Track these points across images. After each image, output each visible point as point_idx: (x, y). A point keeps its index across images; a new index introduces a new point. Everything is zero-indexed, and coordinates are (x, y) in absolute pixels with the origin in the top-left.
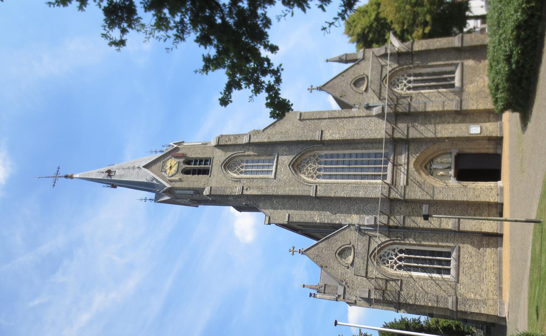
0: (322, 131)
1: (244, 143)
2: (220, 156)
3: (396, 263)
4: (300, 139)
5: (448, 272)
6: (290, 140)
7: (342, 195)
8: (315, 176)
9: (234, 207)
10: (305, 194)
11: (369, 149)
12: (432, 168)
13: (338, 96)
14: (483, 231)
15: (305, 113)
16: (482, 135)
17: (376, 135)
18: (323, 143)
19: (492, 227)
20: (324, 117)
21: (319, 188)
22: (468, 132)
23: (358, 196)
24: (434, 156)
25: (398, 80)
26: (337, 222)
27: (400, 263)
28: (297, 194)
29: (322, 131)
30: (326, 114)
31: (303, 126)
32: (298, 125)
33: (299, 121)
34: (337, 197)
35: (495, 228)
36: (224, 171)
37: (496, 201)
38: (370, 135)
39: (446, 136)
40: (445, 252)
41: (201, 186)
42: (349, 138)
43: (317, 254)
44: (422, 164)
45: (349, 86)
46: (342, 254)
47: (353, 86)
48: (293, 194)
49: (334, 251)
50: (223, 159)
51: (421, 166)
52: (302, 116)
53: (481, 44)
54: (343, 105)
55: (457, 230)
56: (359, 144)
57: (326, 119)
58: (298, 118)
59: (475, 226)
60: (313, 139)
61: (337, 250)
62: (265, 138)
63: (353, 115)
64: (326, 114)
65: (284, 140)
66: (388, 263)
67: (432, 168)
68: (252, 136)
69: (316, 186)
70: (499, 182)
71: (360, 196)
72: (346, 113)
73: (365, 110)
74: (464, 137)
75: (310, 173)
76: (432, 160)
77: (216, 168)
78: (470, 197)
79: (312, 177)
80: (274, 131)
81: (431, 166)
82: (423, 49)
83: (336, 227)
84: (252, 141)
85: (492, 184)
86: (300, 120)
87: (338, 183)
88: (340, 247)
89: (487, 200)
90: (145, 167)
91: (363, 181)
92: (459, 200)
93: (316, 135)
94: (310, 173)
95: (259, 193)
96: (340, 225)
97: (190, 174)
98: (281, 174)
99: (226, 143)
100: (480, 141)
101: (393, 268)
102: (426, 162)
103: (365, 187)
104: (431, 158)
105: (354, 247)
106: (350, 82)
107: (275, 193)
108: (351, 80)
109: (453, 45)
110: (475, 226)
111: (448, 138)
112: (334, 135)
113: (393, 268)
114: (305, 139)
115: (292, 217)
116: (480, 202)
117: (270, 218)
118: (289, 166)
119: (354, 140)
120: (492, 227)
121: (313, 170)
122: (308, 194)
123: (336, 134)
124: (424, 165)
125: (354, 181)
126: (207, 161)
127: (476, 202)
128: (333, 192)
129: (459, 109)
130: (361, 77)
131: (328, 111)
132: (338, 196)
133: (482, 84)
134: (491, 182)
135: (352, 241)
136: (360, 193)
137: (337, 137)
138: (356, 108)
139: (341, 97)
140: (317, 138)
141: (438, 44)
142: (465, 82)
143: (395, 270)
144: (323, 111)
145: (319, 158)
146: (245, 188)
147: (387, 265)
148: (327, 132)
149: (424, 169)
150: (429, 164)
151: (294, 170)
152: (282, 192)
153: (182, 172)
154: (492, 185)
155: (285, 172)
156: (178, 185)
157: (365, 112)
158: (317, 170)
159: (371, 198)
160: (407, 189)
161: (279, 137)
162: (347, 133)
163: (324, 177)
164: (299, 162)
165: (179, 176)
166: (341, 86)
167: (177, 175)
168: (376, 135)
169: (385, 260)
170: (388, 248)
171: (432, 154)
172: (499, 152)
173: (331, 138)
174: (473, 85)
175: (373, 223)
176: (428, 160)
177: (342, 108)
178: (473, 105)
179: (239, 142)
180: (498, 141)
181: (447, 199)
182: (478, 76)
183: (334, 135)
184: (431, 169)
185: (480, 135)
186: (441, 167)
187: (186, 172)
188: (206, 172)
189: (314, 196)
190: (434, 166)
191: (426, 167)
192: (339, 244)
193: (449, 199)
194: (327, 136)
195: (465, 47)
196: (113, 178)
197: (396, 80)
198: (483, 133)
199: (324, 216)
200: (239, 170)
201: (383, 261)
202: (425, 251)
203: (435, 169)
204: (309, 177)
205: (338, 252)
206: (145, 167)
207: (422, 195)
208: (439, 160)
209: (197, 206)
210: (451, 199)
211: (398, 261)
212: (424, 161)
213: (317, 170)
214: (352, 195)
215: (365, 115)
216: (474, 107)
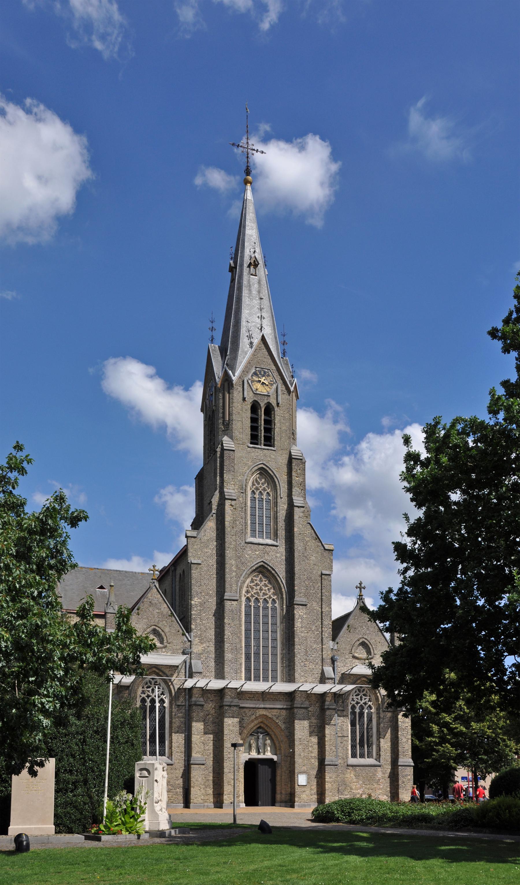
0: (306, 605)
1: (294, 498)
2: (275, 459)
3: (148, 696)
4: (296, 576)
5: (354, 756)
6: (296, 564)
7: (226, 632)
8: (249, 595)
9: (202, 469)
10: (227, 586)
11: (282, 663)
12: (259, 734)
13: (350, 621)
14: (192, 789)
15: (330, 581)
16: (296, 787)
17: (299, 671)
18: (291, 605)
19: (196, 798)
20: (323, 606)
21: (234, 603)
22: (300, 773)
23: (226, 652)
24: (273, 736)
25: (364, 695)
26: (193, 627)
27: (148, 701)
28: (227, 576)
29: (306, 605)
30: (327, 609)
31: (313, 578)
32: (314, 572)
33: (320, 573)
34: (224, 627)
35: (195, 801)
36: (256, 468)
37: (225, 801)
38: (299, 665)
39: (296, 750)
40: (164, 750)
41: (236, 433)
42: (296, 640)
43: (153, 602)
44: (264, 724)
45: (360, 636)
46: (155, 633)
47: (361, 641)
48: (227, 570)
49: (158, 623)
50: (272, 465)
51: (261, 722)
52: (326, 577)
53: (400, 786)
54: (339, 624)
55: (192, 762)
56: (289, 650)
57: (322, 608)
58: (324, 572)
59: (197, 781)
60: (296, 593)
61: (158, 627)
62: (299, 528)
63: (324, 643)
64: (327, 609)
65: (296, 554)
66: (147, 688)
67: (259, 734)
68: (302, 509)
69: (237, 600)
70: (244, 804)
71: (226, 654)
72: (328, 631)
73: (330, 656)
74: (294, 769)
75: (252, 588)
76: (268, 734)
77: (261, 455)
78: (228, 776)
79: (248, 592)
80: (307, 539)
81: (261, 733)
82: (400, 723)
83: (186, 622)
84: (296, 509)
85: (242, 798)
86: (322, 574)
87: (240, 625)
88: (163, 631)
89: (225, 793)
90: (263, 336)
91: (243, 656)
92: (225, 764)
93: (301, 597)
94: (252, 588)
95: (227, 523)
96: (188, 629)
97: (251, 413)
98: (252, 550)
99: (294, 470)
100: (289, 785)
101: (141, 693)
102: (266, 728)
103: (236, 660)
104: (271, 733)
105: (166, 647)
106: (366, 637)
107: (227, 545)
108: (369, 639)
109: (401, 756)
110: (197, 781)
111: (294, 752)
112: (300, 620)
113: (141, 693)
114: (296, 582)
115: (197, 568)
116: (223, 786)
117: (194, 537)
118: (262, 561)
119: (293, 645)
120: (196, 798)
121: (257, 593)
122: (226, 590)
123: (301, 622)
124: (262, 725)
125: (243, 645)
126: (269, 441)
127: (223, 782)
128: (230, 621)
129: (326, 763)
130: (372, 651)
131: (331, 611)
132: (226, 628)
133: (354, 787)
134: (243, 796)
135: (171, 645)
136: (230, 655)
137: (298, 624)
138: (334, 646)
139: (348, 626)
140: (297, 599)
141: (404, 740)
142: (358, 768)
143: (140, 696)
144: (331, 604)
145: (271, 600)
146: (233, 503)
147: (145, 687)
148: (305, 611)
149: (258, 726)
150: (263, 731)
151: (257, 568)
152: (229, 555)
153: (255, 400)
154: (241, 798)
155: (253, 557)
156: (237, 394)
157: (328, 655)
158: (257, 599)
159: (223, 668)
160: (235, 709)
161: (300, 548)
162: (302, 637)
163: (248, 607)
164: (268, 574)
165: (250, 397)
166: (362, 627)
167: (251, 394)
168: (299, 671)
169: (151, 684)
170: (165, 687)
171: (275, 735)
172: (277, 804)
173: (297, 617)
174: (354, 777)
175: (194, 671)
176: (268, 730)
177: (334, 622)
178: (330, 778)
179: (296, 490)
180: (290, 802)
181: (225, 751)
182: (364, 782)
183: (300, 620)
184: (257, 733)
185: (296, 785)
186: (260, 744)
187: (255, 407)
188: (254, 439)
189: (225, 598)
190: (261, 736)
191: (260, 727)
192: (167, 630)
193: (225, 754)
194: (299, 612)
195: (398, 769)
196: (246, 270)
197: (364, 693)
198: (299, 788)
199: (200, 610)
200: (257, 489)
201: (150, 681)
202: (165, 728)
203: (258, 738)
204: (247, 587)
205: (157, 628)
206: (263, 336)
207: (229, 725)
208: (268, 742)
209: (202, 410)
210: (225, 756)
211: (150, 698)
212: (267, 726)
213: (257, 599)
214: (227, 645)
215: (324, 657)
216: (327, 779)
